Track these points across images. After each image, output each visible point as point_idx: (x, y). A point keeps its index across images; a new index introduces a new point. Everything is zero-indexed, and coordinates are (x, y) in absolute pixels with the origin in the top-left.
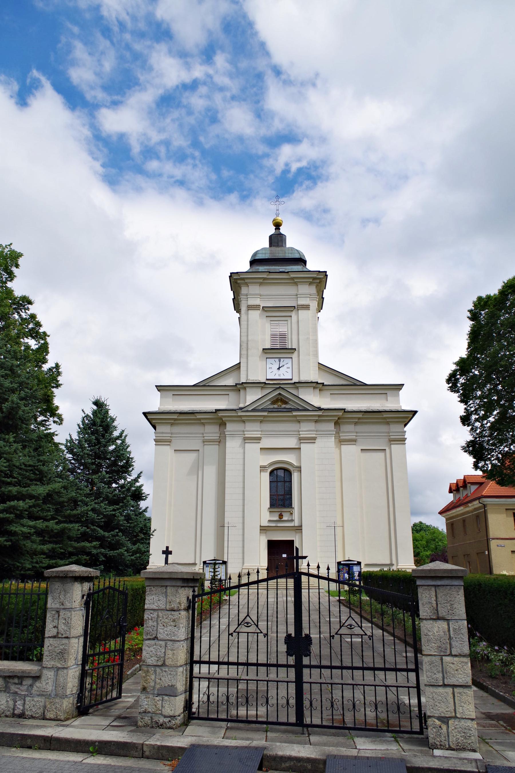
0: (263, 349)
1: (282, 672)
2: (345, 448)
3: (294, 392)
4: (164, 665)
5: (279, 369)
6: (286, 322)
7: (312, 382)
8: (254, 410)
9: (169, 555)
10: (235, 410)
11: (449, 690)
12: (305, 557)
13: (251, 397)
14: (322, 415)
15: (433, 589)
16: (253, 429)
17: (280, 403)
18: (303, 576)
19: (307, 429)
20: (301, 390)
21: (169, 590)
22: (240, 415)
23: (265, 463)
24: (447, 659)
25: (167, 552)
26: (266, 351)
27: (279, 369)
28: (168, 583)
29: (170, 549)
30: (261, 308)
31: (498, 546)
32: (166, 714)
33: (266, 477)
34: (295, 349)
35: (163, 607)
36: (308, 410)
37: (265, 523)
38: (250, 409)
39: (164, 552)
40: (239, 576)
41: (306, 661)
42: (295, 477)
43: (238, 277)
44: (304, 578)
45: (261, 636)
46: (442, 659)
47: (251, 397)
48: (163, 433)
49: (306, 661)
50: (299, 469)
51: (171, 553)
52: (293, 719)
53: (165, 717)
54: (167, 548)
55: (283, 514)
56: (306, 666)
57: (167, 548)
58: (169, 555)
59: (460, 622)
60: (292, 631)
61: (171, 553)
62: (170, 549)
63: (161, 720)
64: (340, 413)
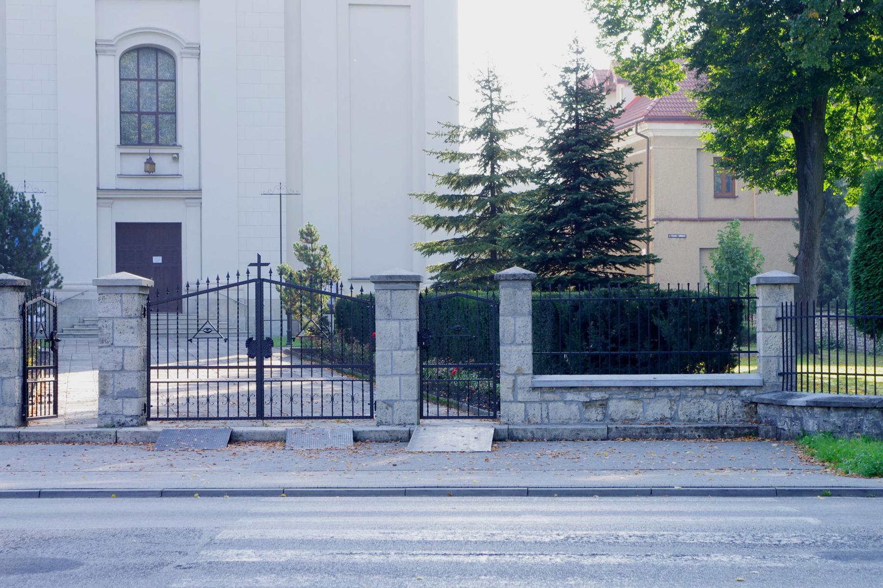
1: (243, 372)
4: (122, 369)
11: (397, 378)
12: (267, 264)
15: (389, 293)
18: (265, 283)
21: (124, 298)
24: (395, 353)
28: (123, 291)
31: (670, 237)
32: (128, 414)
33: (110, 67)
35: (119, 314)
37: (109, 182)
40: (198, 283)
41: (267, 362)
42: (185, 69)
44: (266, 285)
45: (222, 342)
46: (392, 354)
49: (267, 362)
50: (196, 51)
52: (253, 412)
53: (126, 417)
55: (155, 159)
56: (267, 367)
59: (410, 322)
60: (253, 333)
63: (123, 420)
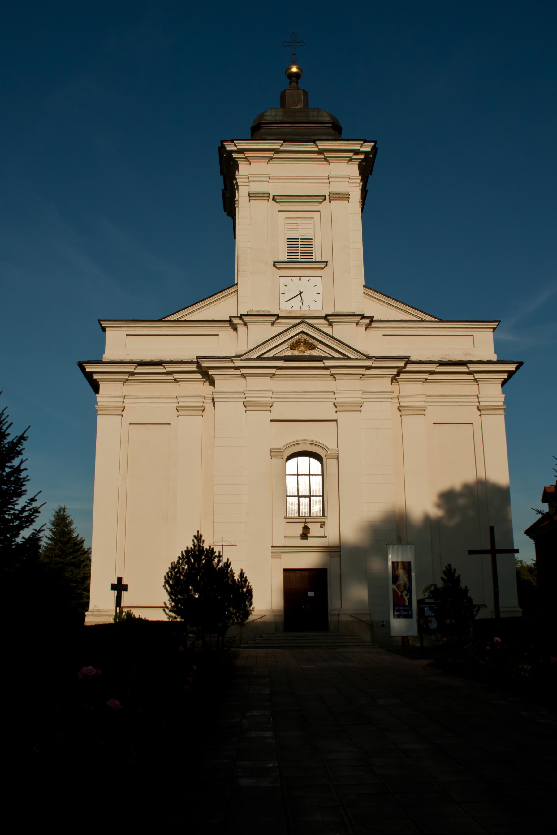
0: (275, 262)
2: (410, 421)
3: (327, 329)
5: (301, 293)
6: (311, 221)
7: (353, 315)
8: (259, 358)
9: (124, 593)
10: (229, 358)
13: (256, 334)
14: (370, 364)
16: (258, 386)
17: (302, 348)
19: (349, 386)
20: (336, 327)
22: (238, 366)
23: (279, 445)
25: (119, 587)
26: (278, 265)
27: (301, 293)
29: (124, 583)
30: (271, 197)
34: (326, 263)
36: (349, 358)
38: (255, 356)
39: (113, 587)
43: (235, 148)
47: (256, 334)
48: (110, 396)
51: (125, 588)
54: (120, 579)
55: (309, 525)
57: (120, 579)
58: (124, 593)
61: (125, 588)
62: (124, 583)
64: (401, 364)
